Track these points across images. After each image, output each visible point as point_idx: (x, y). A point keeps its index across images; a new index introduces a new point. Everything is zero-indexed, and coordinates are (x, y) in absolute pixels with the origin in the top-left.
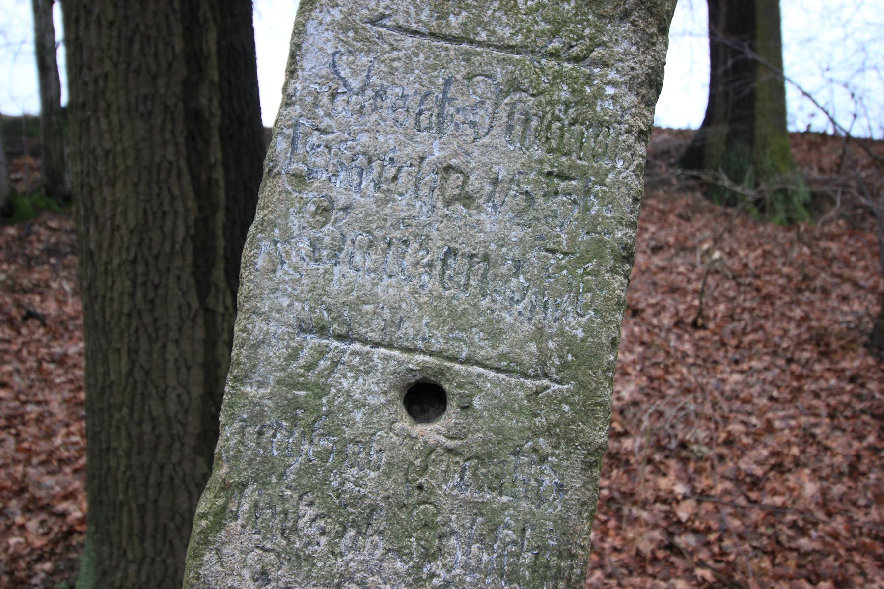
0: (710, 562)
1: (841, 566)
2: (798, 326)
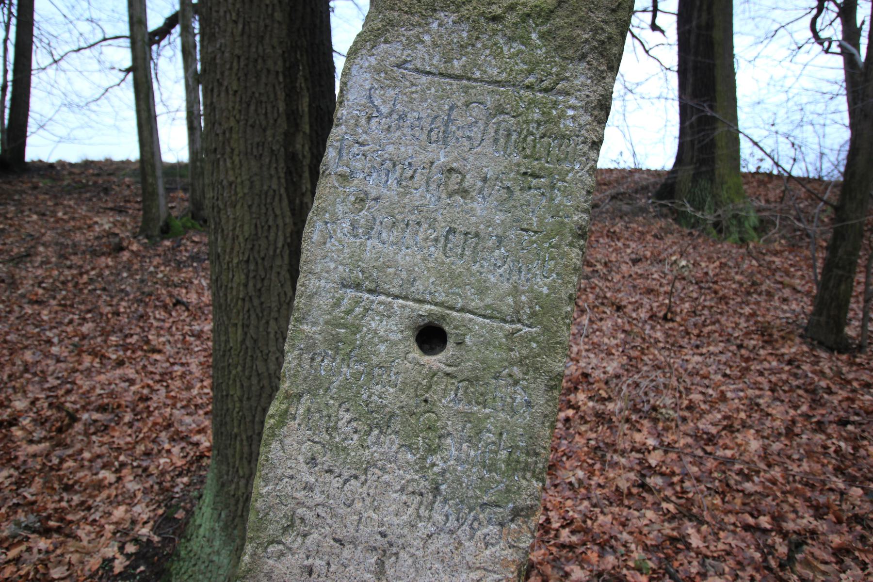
0: (674, 498)
1: (778, 505)
2: (747, 321)
